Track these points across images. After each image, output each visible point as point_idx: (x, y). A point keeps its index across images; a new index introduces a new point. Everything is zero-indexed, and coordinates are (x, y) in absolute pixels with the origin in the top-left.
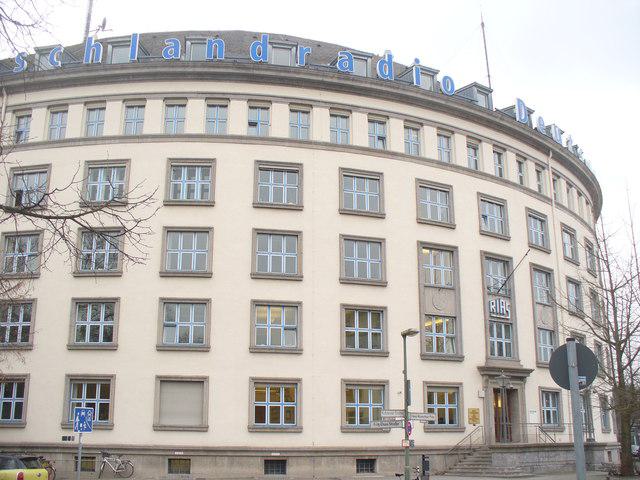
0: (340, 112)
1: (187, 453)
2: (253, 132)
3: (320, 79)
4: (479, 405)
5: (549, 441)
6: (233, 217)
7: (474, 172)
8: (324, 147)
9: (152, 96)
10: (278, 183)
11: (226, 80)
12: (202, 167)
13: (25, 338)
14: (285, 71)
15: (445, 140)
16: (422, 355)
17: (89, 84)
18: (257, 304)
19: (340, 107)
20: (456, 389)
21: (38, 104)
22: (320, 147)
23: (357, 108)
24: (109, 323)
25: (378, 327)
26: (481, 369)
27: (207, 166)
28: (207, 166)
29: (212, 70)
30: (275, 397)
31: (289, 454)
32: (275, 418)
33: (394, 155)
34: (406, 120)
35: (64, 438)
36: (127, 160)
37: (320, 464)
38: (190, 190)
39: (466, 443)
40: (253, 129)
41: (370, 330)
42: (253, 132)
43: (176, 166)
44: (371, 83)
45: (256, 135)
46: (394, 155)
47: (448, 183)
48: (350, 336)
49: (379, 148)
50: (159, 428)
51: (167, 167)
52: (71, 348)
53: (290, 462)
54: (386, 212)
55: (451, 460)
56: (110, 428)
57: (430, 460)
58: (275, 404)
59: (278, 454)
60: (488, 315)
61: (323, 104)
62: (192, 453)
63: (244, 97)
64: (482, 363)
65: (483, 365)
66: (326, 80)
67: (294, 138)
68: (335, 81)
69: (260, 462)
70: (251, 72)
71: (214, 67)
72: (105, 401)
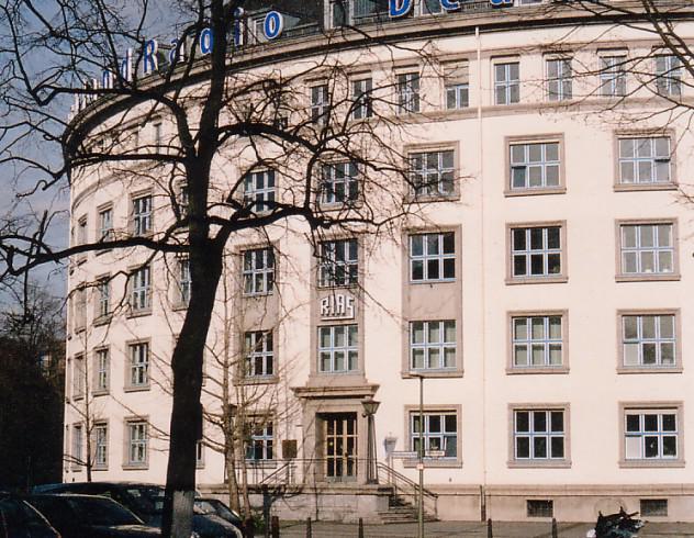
47: (558, 132)
56: (568, 466)
72: (523, 435)
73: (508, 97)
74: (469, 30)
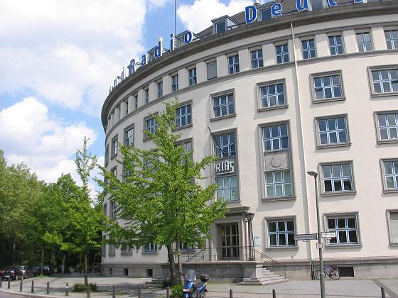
0: (363, 31)
7: (137, 110)
17: (250, 36)
21: (198, 61)
24: (273, 233)
30: (281, 229)
32: (283, 242)
34: (384, 26)
49: (338, 51)
56: (360, 247)
58: (282, 233)
69: (144, 270)
73: (258, 65)
74: (287, 26)
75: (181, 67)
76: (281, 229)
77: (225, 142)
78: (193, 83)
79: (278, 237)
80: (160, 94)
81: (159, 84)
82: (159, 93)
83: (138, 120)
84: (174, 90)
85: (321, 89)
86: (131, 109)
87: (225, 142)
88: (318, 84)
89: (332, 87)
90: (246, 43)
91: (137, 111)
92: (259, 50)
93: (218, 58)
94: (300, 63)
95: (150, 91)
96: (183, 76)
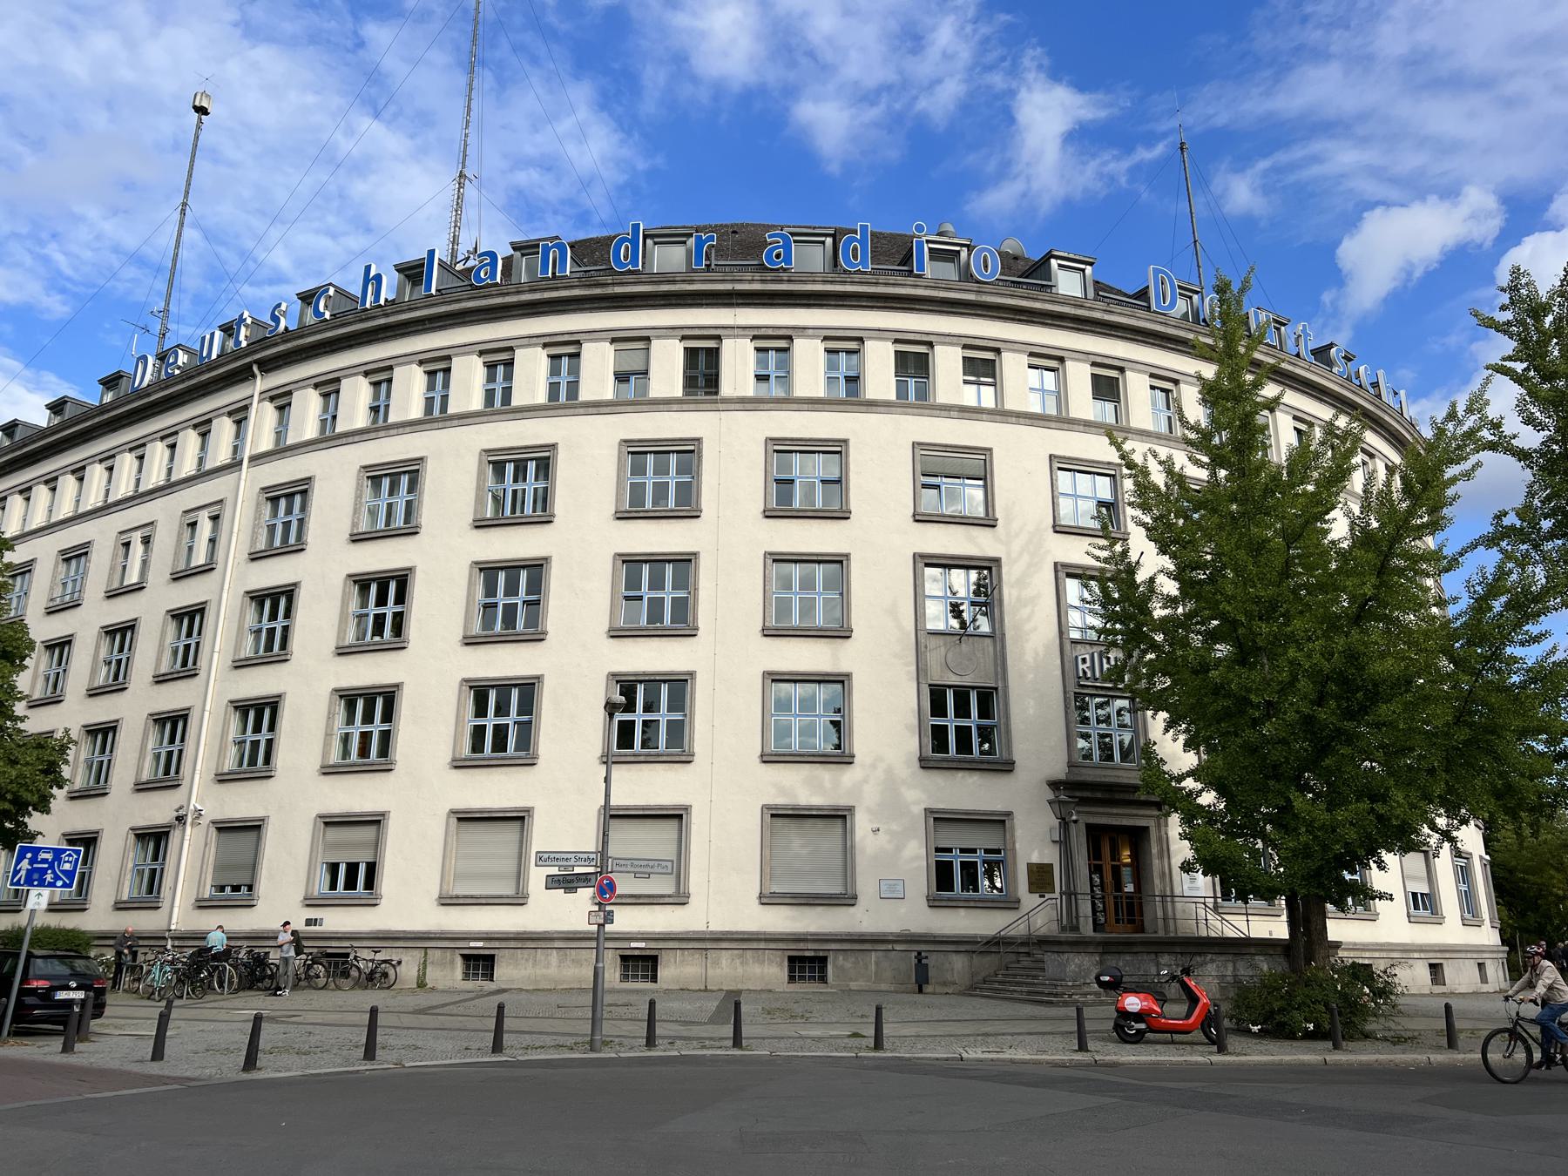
1: (653, 945)
2: (764, 390)
3: (728, 287)
4: (1047, 854)
5: (1230, 933)
6: (584, 540)
7: (330, 437)
8: (738, 406)
9: (948, 339)
10: (662, 480)
11: (574, 311)
12: (655, 452)
13: (384, 751)
14: (669, 282)
15: (1049, 376)
16: (921, 760)
17: (334, 351)
18: (775, 678)
19: (770, 332)
20: (999, 821)
22: (733, 406)
23: (802, 330)
24: (480, 722)
25: (681, 708)
26: (1054, 785)
27: (688, 452)
28: (688, 452)
29: (547, 295)
30: (962, 710)
31: (661, 945)
33: (873, 405)
35: (309, 922)
36: (421, 459)
37: (717, 963)
38: (661, 490)
39: (1020, 930)
40: (764, 385)
41: (951, 722)
42: (764, 390)
43: (636, 452)
44: (825, 282)
45: (774, 387)
46: (873, 405)
48: (939, 734)
50: (447, 901)
51: (480, 462)
52: (458, 765)
53: (664, 959)
54: (853, 506)
55: (987, 963)
57: (932, 961)
59: (642, 945)
60: (1071, 682)
61: (741, 332)
62: (497, 944)
63: (604, 335)
64: (1059, 770)
65: (1062, 776)
66: (739, 287)
67: (833, 396)
68: (757, 287)
70: (609, 290)
71: (566, 288)
73: (774, 387)
75: (405, 359)
76: (962, 710)
77: (512, 590)
78: (437, 414)
79: (974, 712)
80: (280, 435)
81: (204, 435)
82: (236, 448)
83: (248, 485)
84: (375, 421)
85: (495, 605)
86: (221, 453)
87: (512, 590)
88: (633, 582)
89: (668, 595)
90: (409, 350)
91: (377, 430)
92: (571, 356)
93: (396, 370)
94: (745, 404)
95: (212, 436)
96: (308, 406)
